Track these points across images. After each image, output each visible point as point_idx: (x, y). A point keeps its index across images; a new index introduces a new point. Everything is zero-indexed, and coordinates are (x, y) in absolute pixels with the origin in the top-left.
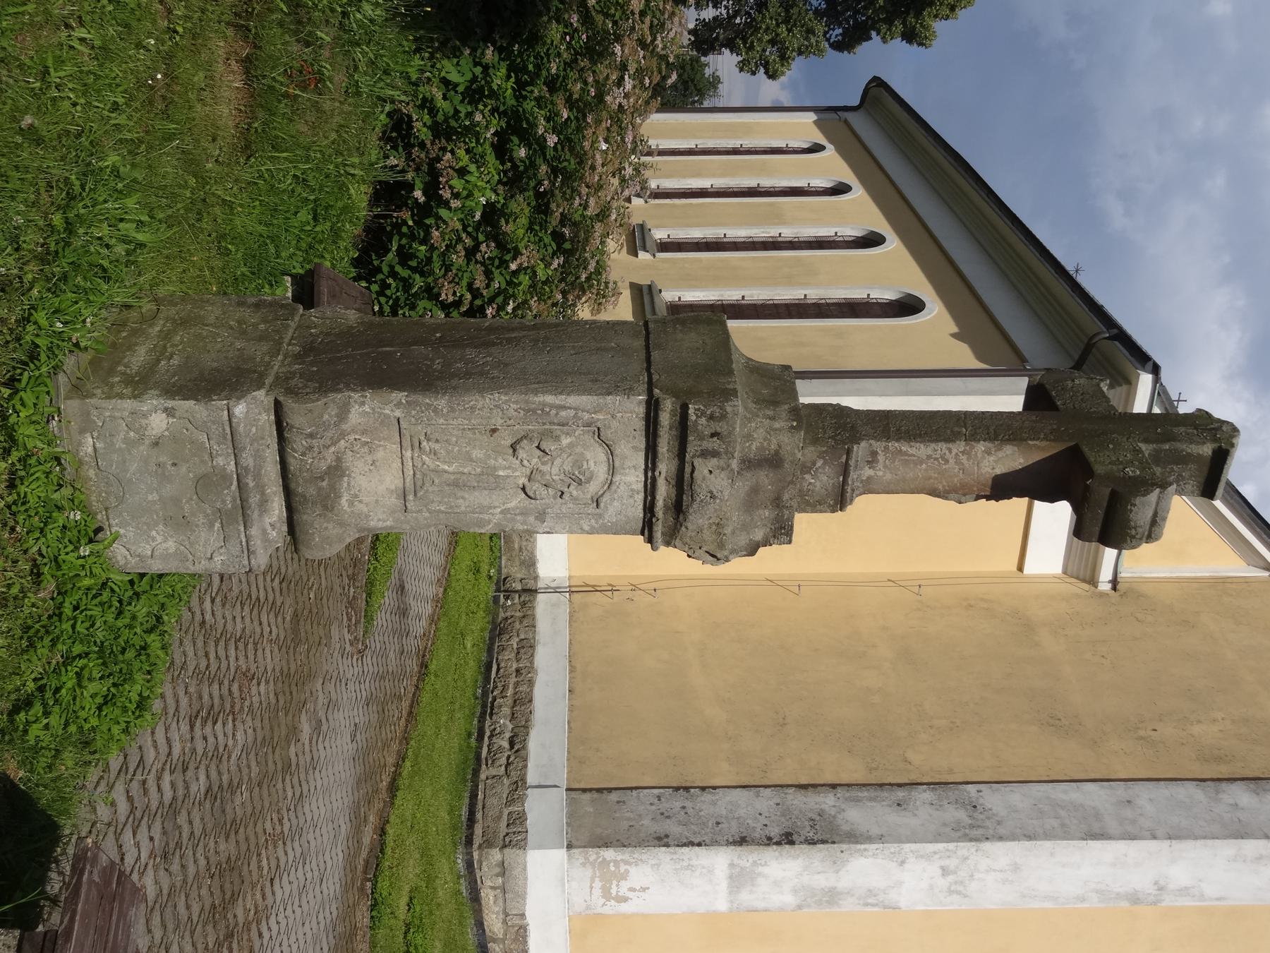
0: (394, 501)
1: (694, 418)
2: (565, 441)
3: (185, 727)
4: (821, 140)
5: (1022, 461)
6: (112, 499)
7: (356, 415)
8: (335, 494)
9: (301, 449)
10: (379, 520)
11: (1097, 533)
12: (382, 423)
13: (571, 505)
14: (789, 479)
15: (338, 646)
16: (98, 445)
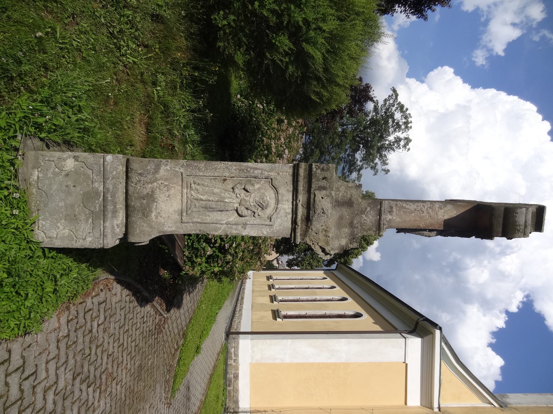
0: (176, 217)
1: (315, 170)
2: (257, 186)
3: (69, 376)
4: (326, 277)
5: (455, 212)
6: (42, 205)
7: (162, 172)
8: (149, 209)
9: (135, 181)
10: (169, 227)
11: (501, 232)
12: (174, 175)
13: (258, 220)
14: (356, 212)
15: (159, 395)
16: (40, 175)
